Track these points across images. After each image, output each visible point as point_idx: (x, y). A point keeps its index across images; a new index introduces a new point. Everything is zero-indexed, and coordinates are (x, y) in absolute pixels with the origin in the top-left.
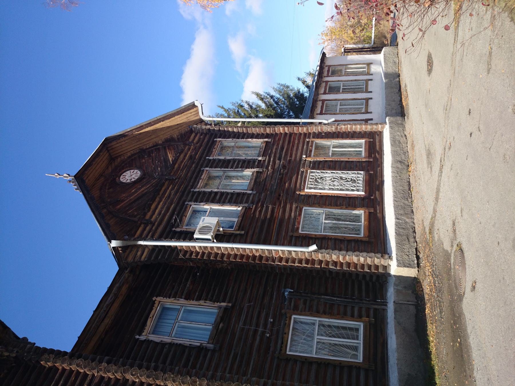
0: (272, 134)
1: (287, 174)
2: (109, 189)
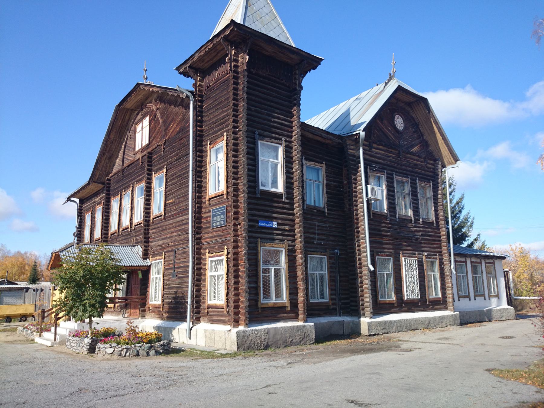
0: (439, 226)
1: (412, 242)
2: (389, 109)
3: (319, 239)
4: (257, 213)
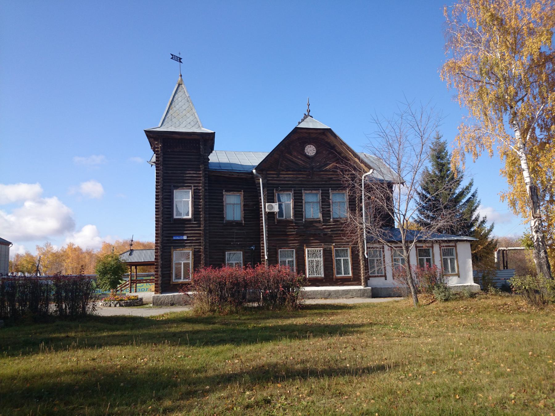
3: (236, 241)
4: (172, 232)
